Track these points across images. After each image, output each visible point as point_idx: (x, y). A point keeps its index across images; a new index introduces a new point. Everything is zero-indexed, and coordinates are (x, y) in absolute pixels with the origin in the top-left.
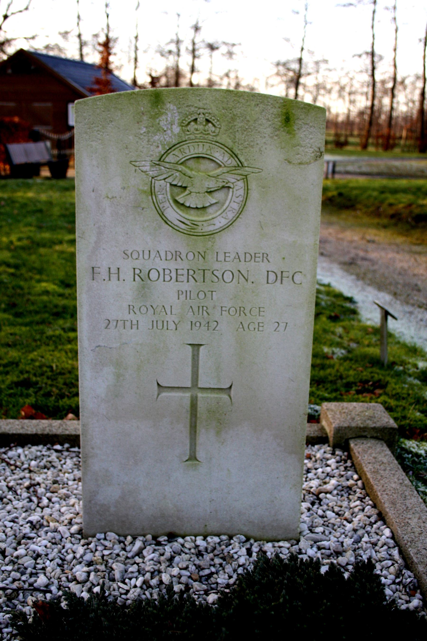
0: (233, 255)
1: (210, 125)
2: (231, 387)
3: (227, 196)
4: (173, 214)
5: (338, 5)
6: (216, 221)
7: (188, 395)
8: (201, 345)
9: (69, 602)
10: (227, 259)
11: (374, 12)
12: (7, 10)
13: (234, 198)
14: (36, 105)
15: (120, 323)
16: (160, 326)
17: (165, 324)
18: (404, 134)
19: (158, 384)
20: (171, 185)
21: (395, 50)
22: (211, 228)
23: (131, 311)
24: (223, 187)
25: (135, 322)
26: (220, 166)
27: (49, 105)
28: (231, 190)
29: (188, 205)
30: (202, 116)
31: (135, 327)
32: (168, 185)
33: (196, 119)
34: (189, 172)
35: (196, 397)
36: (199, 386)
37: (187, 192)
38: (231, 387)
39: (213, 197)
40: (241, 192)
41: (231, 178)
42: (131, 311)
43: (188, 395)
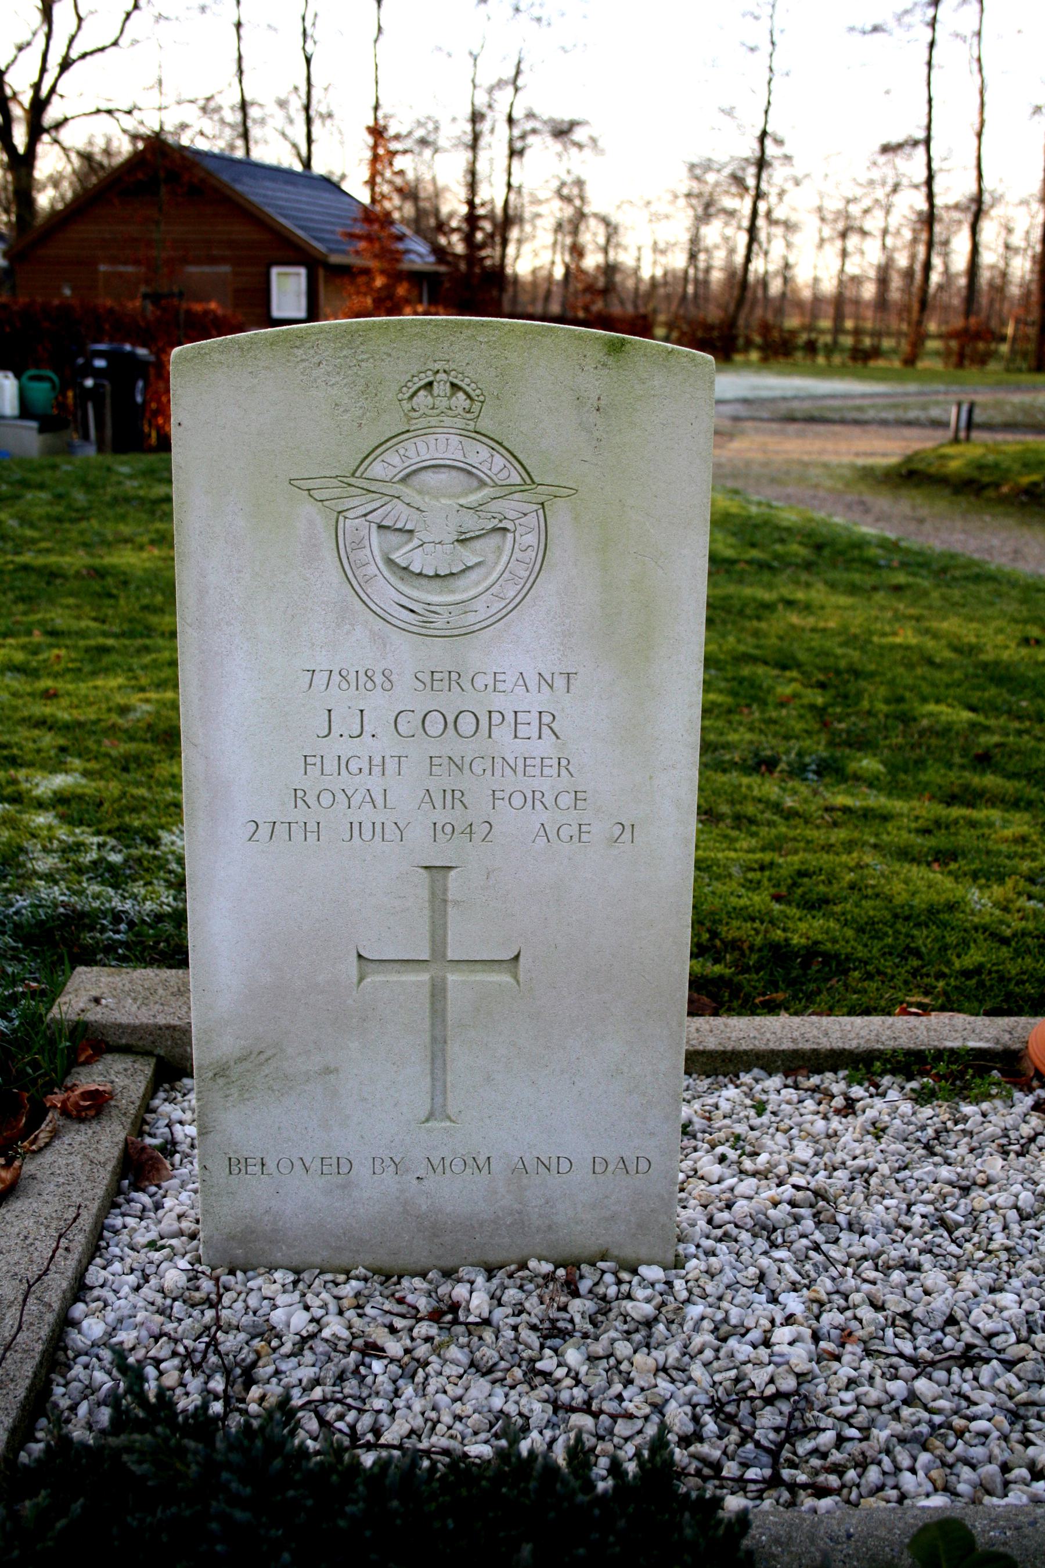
0: (511, 678)
1: (461, 395)
2: (517, 957)
3: (500, 550)
4: (386, 592)
5: (852, 29)
6: (479, 605)
7: (425, 977)
8: (450, 868)
9: (673, 1492)
10: (500, 686)
11: (932, 45)
12: (69, 47)
13: (518, 554)
14: (192, 269)
15: (281, 830)
16: (367, 834)
17: (378, 829)
18: (1010, 331)
19: (360, 956)
20: (380, 527)
21: (979, 135)
22: (471, 618)
23: (300, 802)
24: (495, 530)
25: (312, 826)
26: (483, 484)
27: (225, 269)
28: (510, 535)
29: (416, 568)
30: (442, 376)
31: (312, 837)
32: (374, 527)
33: (430, 384)
34: (417, 500)
35: (444, 980)
36: (451, 955)
37: (416, 542)
38: (517, 957)
39: (474, 552)
40: (531, 539)
41: (511, 507)
42: (300, 802)
43: (425, 977)
